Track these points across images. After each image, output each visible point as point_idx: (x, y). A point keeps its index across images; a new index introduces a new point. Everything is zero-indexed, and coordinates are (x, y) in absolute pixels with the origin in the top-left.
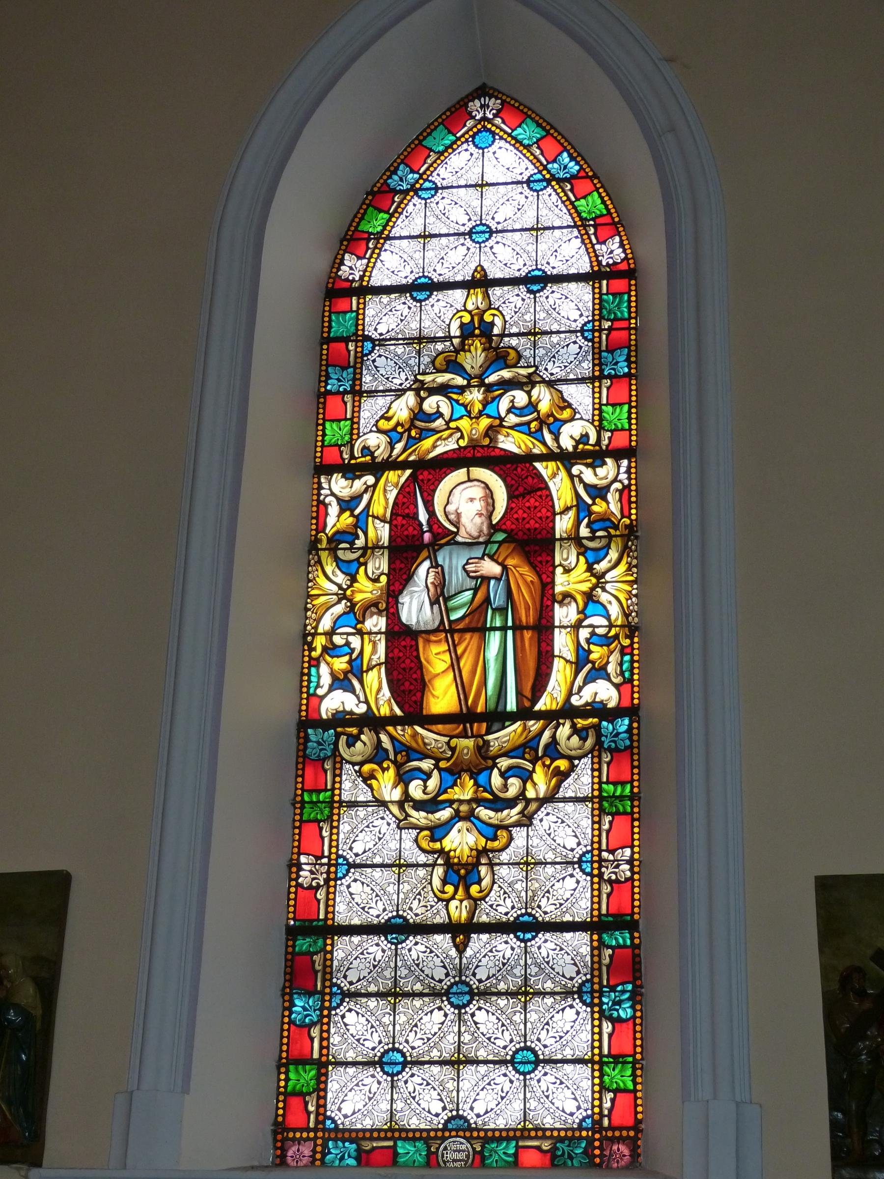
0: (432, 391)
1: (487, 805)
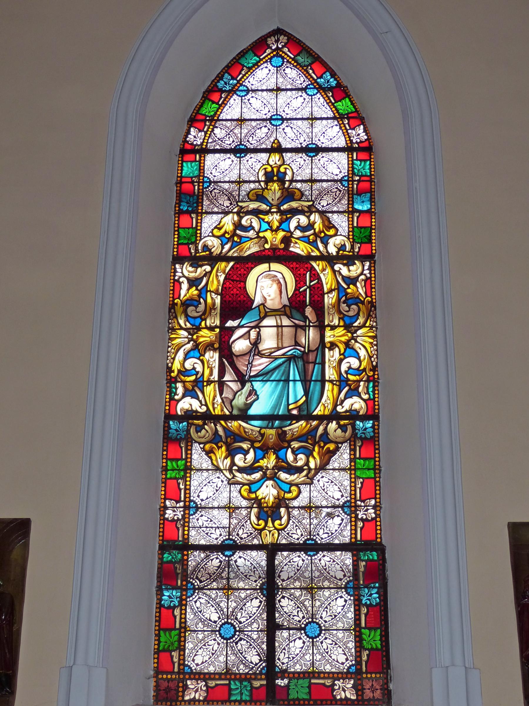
0: (248, 213)
1: (282, 204)
